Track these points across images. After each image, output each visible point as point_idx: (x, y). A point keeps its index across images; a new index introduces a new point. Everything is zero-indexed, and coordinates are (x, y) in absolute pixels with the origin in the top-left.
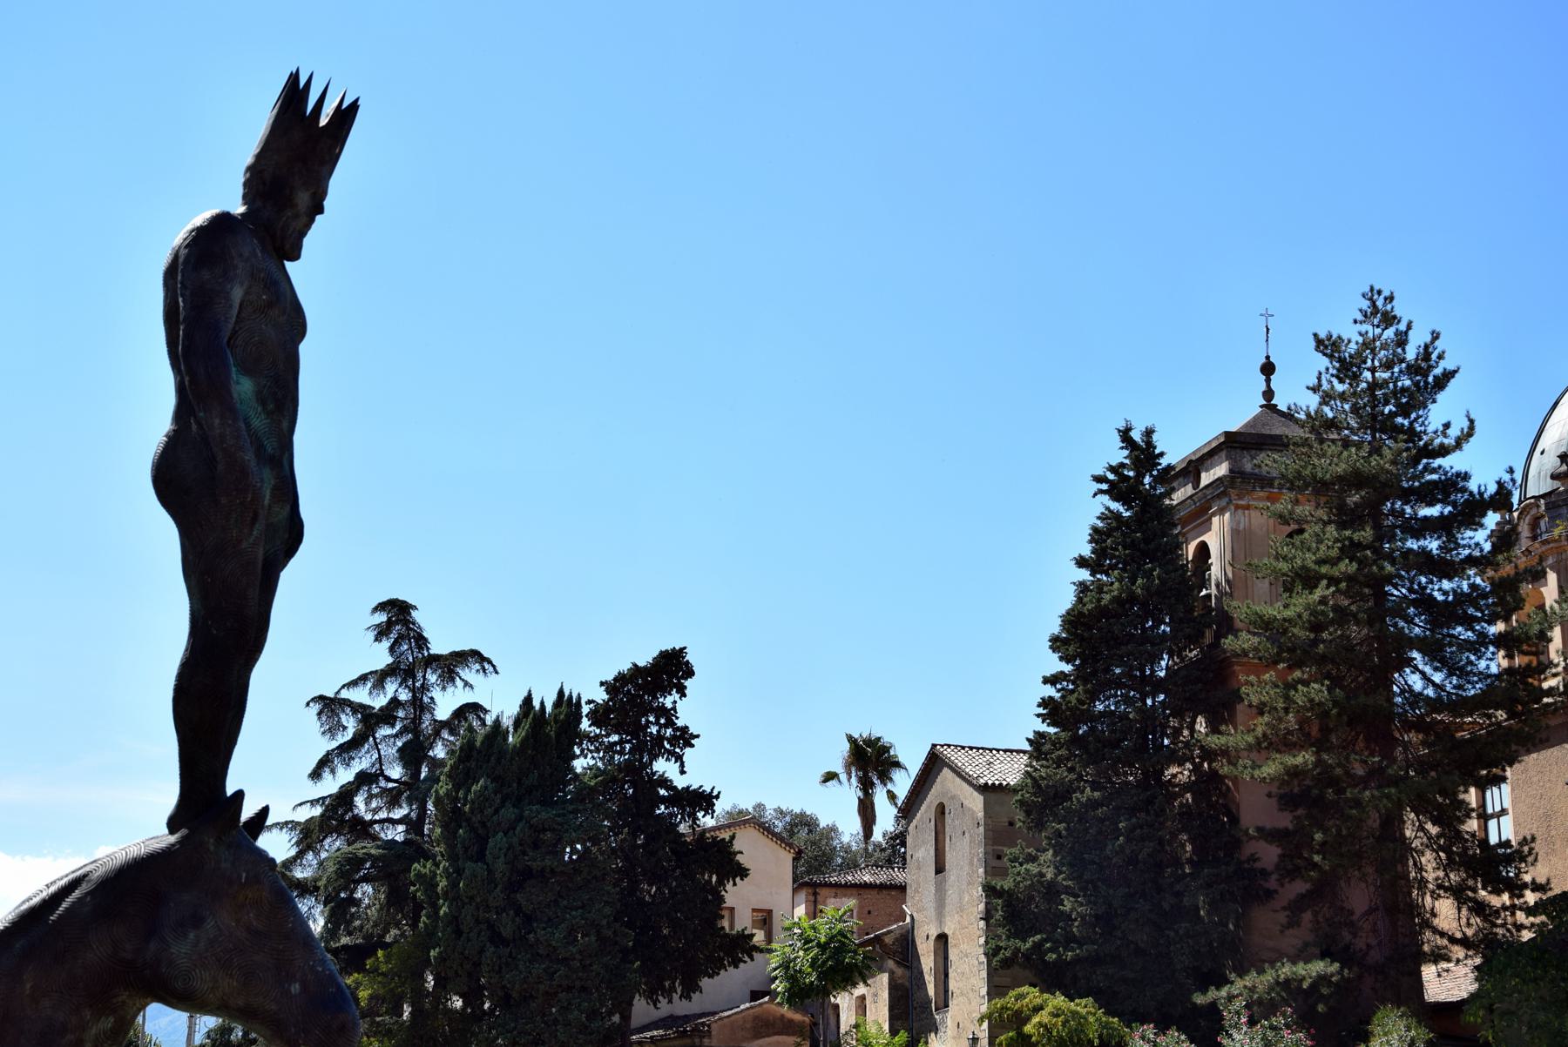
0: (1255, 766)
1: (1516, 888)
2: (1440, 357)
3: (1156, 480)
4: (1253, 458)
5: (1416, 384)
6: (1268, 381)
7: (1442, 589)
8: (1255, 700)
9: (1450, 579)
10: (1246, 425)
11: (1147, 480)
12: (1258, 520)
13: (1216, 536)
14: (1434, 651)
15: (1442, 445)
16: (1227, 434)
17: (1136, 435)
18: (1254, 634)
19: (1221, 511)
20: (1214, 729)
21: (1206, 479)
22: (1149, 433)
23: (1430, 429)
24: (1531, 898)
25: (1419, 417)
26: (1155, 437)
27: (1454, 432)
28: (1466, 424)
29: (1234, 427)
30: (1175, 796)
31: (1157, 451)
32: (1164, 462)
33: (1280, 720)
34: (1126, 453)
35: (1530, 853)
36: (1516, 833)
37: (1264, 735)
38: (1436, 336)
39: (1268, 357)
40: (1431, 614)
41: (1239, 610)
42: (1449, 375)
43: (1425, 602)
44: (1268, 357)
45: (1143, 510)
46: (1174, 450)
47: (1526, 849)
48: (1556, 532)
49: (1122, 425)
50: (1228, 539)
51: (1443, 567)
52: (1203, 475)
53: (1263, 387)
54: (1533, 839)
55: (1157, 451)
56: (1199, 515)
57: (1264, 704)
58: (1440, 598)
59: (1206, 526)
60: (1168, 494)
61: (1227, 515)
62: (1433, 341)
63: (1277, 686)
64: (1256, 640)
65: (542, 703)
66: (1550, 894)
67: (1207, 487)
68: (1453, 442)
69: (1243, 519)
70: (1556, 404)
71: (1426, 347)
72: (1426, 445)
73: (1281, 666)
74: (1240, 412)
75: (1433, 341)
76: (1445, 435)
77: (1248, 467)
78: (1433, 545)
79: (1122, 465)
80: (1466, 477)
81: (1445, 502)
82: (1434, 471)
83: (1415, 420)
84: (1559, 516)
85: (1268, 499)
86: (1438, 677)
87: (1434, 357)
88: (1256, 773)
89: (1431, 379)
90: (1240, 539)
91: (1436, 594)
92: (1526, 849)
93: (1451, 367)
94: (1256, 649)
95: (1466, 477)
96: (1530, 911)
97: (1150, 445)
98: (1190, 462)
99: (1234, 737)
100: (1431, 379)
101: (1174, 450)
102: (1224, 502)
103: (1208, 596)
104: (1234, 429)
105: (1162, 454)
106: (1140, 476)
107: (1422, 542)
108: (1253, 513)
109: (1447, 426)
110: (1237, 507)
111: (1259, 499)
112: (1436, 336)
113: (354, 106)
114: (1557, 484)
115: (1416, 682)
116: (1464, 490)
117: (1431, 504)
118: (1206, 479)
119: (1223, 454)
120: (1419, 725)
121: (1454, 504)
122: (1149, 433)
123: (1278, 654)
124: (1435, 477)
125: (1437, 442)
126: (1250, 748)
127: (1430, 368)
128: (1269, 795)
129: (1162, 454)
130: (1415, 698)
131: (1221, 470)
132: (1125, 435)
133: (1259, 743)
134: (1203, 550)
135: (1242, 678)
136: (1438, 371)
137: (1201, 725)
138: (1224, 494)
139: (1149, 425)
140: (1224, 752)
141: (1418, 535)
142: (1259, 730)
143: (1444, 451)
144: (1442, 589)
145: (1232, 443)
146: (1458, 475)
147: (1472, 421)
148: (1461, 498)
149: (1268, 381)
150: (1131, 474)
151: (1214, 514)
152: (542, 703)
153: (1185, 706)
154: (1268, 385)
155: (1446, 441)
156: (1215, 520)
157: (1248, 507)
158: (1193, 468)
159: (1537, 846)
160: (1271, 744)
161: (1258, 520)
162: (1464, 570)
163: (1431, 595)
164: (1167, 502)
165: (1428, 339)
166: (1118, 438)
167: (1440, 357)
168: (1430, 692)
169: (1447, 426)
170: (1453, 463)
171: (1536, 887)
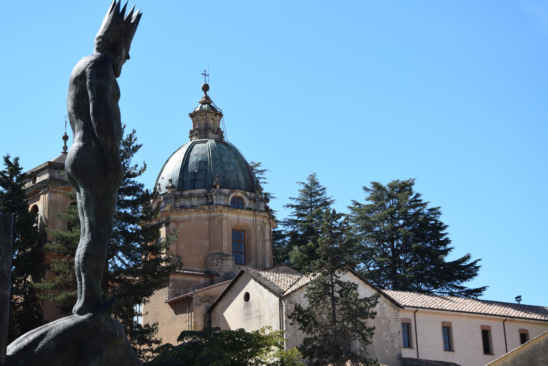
0: (55, 296)
1: (150, 343)
2: (135, 140)
3: (18, 180)
4: (59, 173)
5: (126, 149)
6: (65, 143)
7: (130, 228)
8: (56, 269)
9: (134, 224)
10: (56, 160)
11: (15, 178)
12: (59, 197)
13: (42, 203)
14: (127, 252)
15: (134, 173)
16: (49, 162)
17: (11, 160)
18: (59, 243)
19: (45, 193)
20: (35, 279)
21: (39, 180)
22: (17, 159)
23: (130, 166)
24: (155, 346)
25: (127, 162)
26: (19, 161)
27: (139, 168)
28: (143, 166)
29: (52, 160)
30: (17, 307)
31: (20, 167)
32: (22, 172)
33: (66, 277)
34: (6, 166)
35: (156, 329)
36: (144, 321)
37: (59, 283)
38: (134, 132)
39: (66, 133)
40: (126, 237)
41: (51, 232)
42: (138, 147)
43: (125, 233)
44: (66, 133)
45: (13, 191)
46: (26, 167)
47: (155, 327)
48: (167, 208)
49: (6, 155)
50: (47, 204)
51: (130, 219)
52: (37, 178)
53: (63, 145)
54: (158, 324)
55: (20, 167)
56: (35, 194)
57: (60, 271)
58: (130, 231)
59: (38, 199)
60: (23, 185)
61: (47, 195)
62: (133, 134)
63: (67, 264)
64: (59, 245)
65: (444, 234)
66: (161, 344)
67: (39, 183)
68: (138, 172)
69: (54, 196)
70: (168, 161)
71: (131, 135)
72: (128, 172)
73: (68, 256)
74: (54, 156)
75: (133, 134)
76: (135, 169)
77: (57, 176)
78: (129, 211)
79: (4, 172)
80: (142, 186)
81: (134, 194)
82: (131, 183)
83: (126, 163)
84: (168, 202)
85: (64, 189)
86: (127, 262)
87: (133, 139)
88: (56, 298)
89: (131, 147)
90: (51, 204)
91: (129, 230)
92: (155, 327)
93: (139, 144)
94: (59, 249)
95: (142, 186)
96: (153, 352)
97: (17, 164)
98: (32, 172)
99: (45, 284)
100: (131, 147)
101: (26, 167)
102: (46, 189)
103: (37, 227)
104: (52, 161)
105: (21, 168)
106: (12, 177)
107: (125, 210)
108: (58, 195)
109: (136, 166)
110: (52, 192)
111: (61, 189)
112: (134, 132)
113: (141, 14)
114: (167, 190)
115: (119, 263)
116: (141, 191)
117: (129, 196)
118: (39, 180)
119: (47, 170)
120: (119, 281)
121: (138, 196)
122: (17, 159)
123: (68, 251)
124: (131, 185)
125: (132, 171)
126: (52, 288)
127: (131, 143)
128: (57, 307)
129: (21, 168)
130: (119, 271)
131: (46, 177)
132: (7, 159)
133: (56, 286)
134: (36, 208)
135: (52, 260)
136: (134, 145)
137: (29, 279)
138: (46, 186)
139: (17, 156)
140: (39, 290)
141: (124, 207)
142: (57, 281)
143: (135, 175)
144: (130, 228)
145: (52, 166)
146: (140, 185)
147: (145, 165)
148: (140, 194)
149: (65, 143)
150: (8, 175)
151: (41, 194)
152: (444, 234)
153: (22, 271)
154: (65, 144)
155: (136, 172)
156: (42, 196)
157: (56, 192)
158: (33, 175)
159: (158, 326)
160: (61, 287)
161: (59, 197)
162: (139, 221)
163: (127, 230)
164: (23, 188)
165: (132, 132)
166: (4, 160)
167: (135, 140)
168: (124, 267)
169: (136, 166)
170: (138, 180)
171: (157, 342)
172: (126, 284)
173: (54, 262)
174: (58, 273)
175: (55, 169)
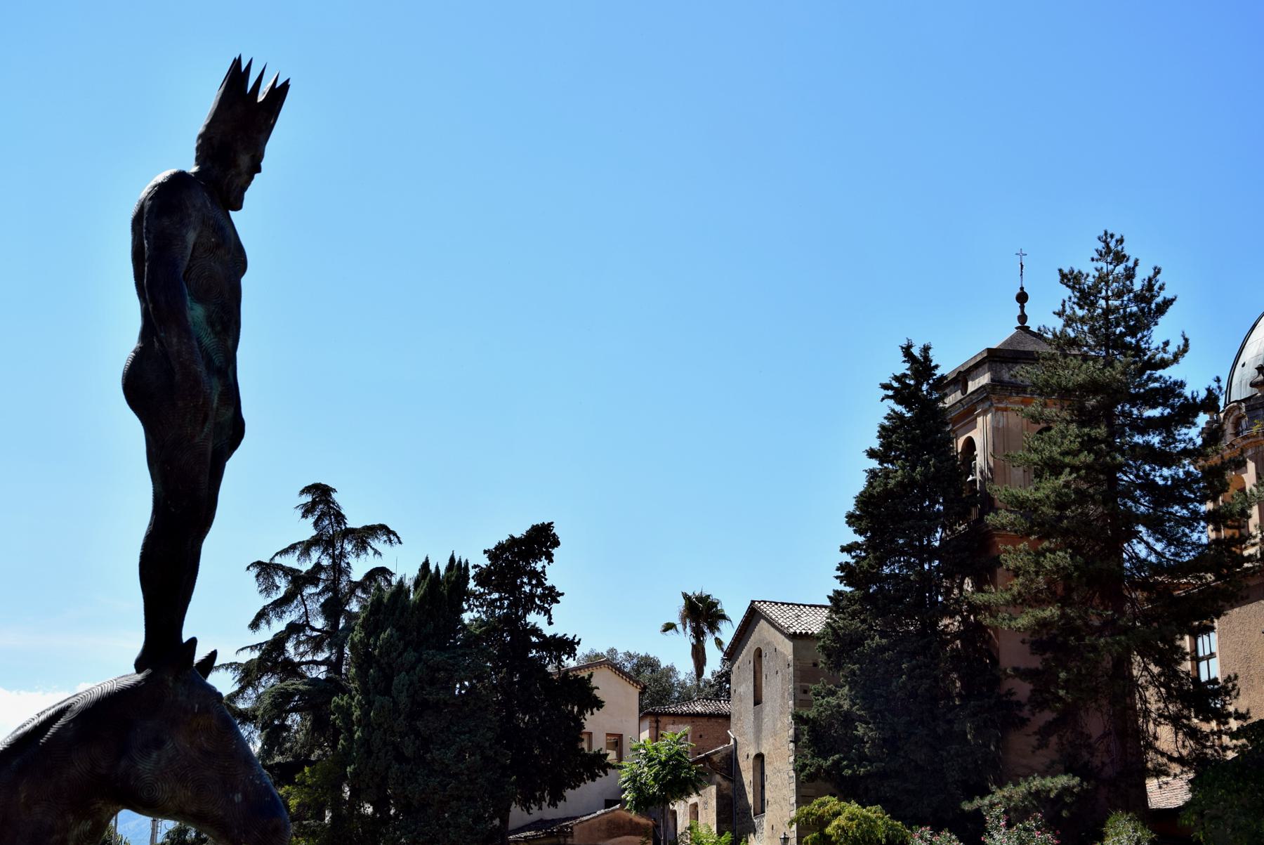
1: (1222, 717)
2: (1161, 288)
3: (932, 387)
4: (1010, 369)
5: (1142, 310)
6: (1022, 307)
7: (1162, 475)
8: (1011, 565)
9: (1169, 467)
10: (1005, 343)
11: (925, 387)
12: (1014, 420)
13: (980, 433)
14: (1155, 525)
15: (1162, 359)
16: (989, 350)
17: (916, 351)
19: (985, 413)
20: (979, 588)
21: (972, 386)
22: (926, 349)
23: (1153, 346)
24: (1234, 724)
25: (1144, 336)
26: (931, 353)
27: (1172, 349)
28: (1182, 342)
29: (995, 344)
31: (933, 364)
32: (938, 373)
33: (1032, 581)
34: (908, 365)
35: (1233, 688)
36: (1222, 672)
37: (1019, 593)
38: (1157, 271)
39: (1022, 289)
41: (999, 492)
42: (1168, 303)
43: (1149, 486)
44: (1022, 289)
46: (946, 363)
47: (1230, 685)
48: (1255, 429)
49: (904, 343)
50: (990, 435)
51: (1164, 458)
52: (970, 383)
53: (1018, 312)
54: (1236, 677)
55: (933, 364)
56: (967, 415)
57: (1019, 568)
58: (1161, 482)
59: (972, 425)
60: (942, 399)
61: (989, 416)
62: (1155, 275)
63: (1029, 554)
64: (1013, 516)
65: (437, 568)
66: (1250, 721)
67: (973, 393)
68: (1171, 357)
69: (1002, 419)
71: (1150, 280)
72: (1150, 359)
73: (1033, 537)
74: (999, 333)
75: (1155, 275)
76: (1165, 351)
77: (1006, 376)
78: (1155, 440)
79: (905, 375)
80: (1182, 385)
81: (1165, 405)
82: (1156, 380)
83: (1141, 339)
84: (1257, 417)
85: (1022, 402)
86: (1159, 547)
87: (1156, 288)
88: (1013, 624)
89: (1153, 306)
90: (999, 435)
91: (1157, 479)
92: (1230, 685)
93: (1170, 296)
94: (1012, 524)
95: (1182, 385)
96: (1233, 736)
97: (927, 359)
99: (994, 595)
100: (1153, 306)
101: (946, 363)
102: (986, 405)
103: (974, 481)
104: (995, 347)
105: (936, 367)
106: (919, 385)
107: (1146, 438)
109: (1166, 344)
110: (998, 409)
111: (1015, 403)
112: (1157, 271)
114: (1255, 391)
115: (1142, 550)
116: (1180, 395)
117: (1153, 407)
118: (972, 386)
119: (986, 367)
120: (1144, 585)
121: (1172, 407)
122: (926, 349)
123: (1031, 528)
124: (1156, 385)
125: (1158, 356)
126: (1007, 603)
127: (1153, 297)
128: (1023, 642)
129: (936, 367)
130: (1140, 563)
131: (984, 379)
132: (907, 351)
133: (1015, 600)
134: (970, 444)
135: (1001, 547)
136: (1159, 300)
137: (968, 585)
138: (987, 398)
139: (926, 343)
140: (987, 607)
141: (1143, 432)
142: (1015, 590)
143: (1164, 364)
144: (1162, 475)
145: (993, 358)
146: (1175, 383)
147: (1186, 340)
148: (1177, 402)
149: (1022, 307)
150: (912, 382)
151: (978, 415)
152: (437, 568)
153: (955, 570)
154: (1022, 311)
155: (1166, 356)
156: (980, 420)
157: (1006, 410)
158: (962, 378)
159: (1239, 683)
160: (1024, 600)
161: (1014, 420)
162: (1180, 460)
163: (1153, 480)
164: (941, 405)
165: (1151, 273)
166: (901, 354)
167: (1161, 288)
168: (1153, 558)
169: (1166, 344)
170: (1171, 373)
171: (1238, 716)
172: (1162, 594)
173: (1006, 551)
174: (1016, 573)
175: (1002, 362)
